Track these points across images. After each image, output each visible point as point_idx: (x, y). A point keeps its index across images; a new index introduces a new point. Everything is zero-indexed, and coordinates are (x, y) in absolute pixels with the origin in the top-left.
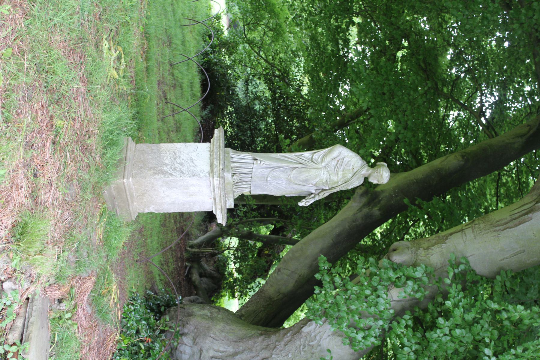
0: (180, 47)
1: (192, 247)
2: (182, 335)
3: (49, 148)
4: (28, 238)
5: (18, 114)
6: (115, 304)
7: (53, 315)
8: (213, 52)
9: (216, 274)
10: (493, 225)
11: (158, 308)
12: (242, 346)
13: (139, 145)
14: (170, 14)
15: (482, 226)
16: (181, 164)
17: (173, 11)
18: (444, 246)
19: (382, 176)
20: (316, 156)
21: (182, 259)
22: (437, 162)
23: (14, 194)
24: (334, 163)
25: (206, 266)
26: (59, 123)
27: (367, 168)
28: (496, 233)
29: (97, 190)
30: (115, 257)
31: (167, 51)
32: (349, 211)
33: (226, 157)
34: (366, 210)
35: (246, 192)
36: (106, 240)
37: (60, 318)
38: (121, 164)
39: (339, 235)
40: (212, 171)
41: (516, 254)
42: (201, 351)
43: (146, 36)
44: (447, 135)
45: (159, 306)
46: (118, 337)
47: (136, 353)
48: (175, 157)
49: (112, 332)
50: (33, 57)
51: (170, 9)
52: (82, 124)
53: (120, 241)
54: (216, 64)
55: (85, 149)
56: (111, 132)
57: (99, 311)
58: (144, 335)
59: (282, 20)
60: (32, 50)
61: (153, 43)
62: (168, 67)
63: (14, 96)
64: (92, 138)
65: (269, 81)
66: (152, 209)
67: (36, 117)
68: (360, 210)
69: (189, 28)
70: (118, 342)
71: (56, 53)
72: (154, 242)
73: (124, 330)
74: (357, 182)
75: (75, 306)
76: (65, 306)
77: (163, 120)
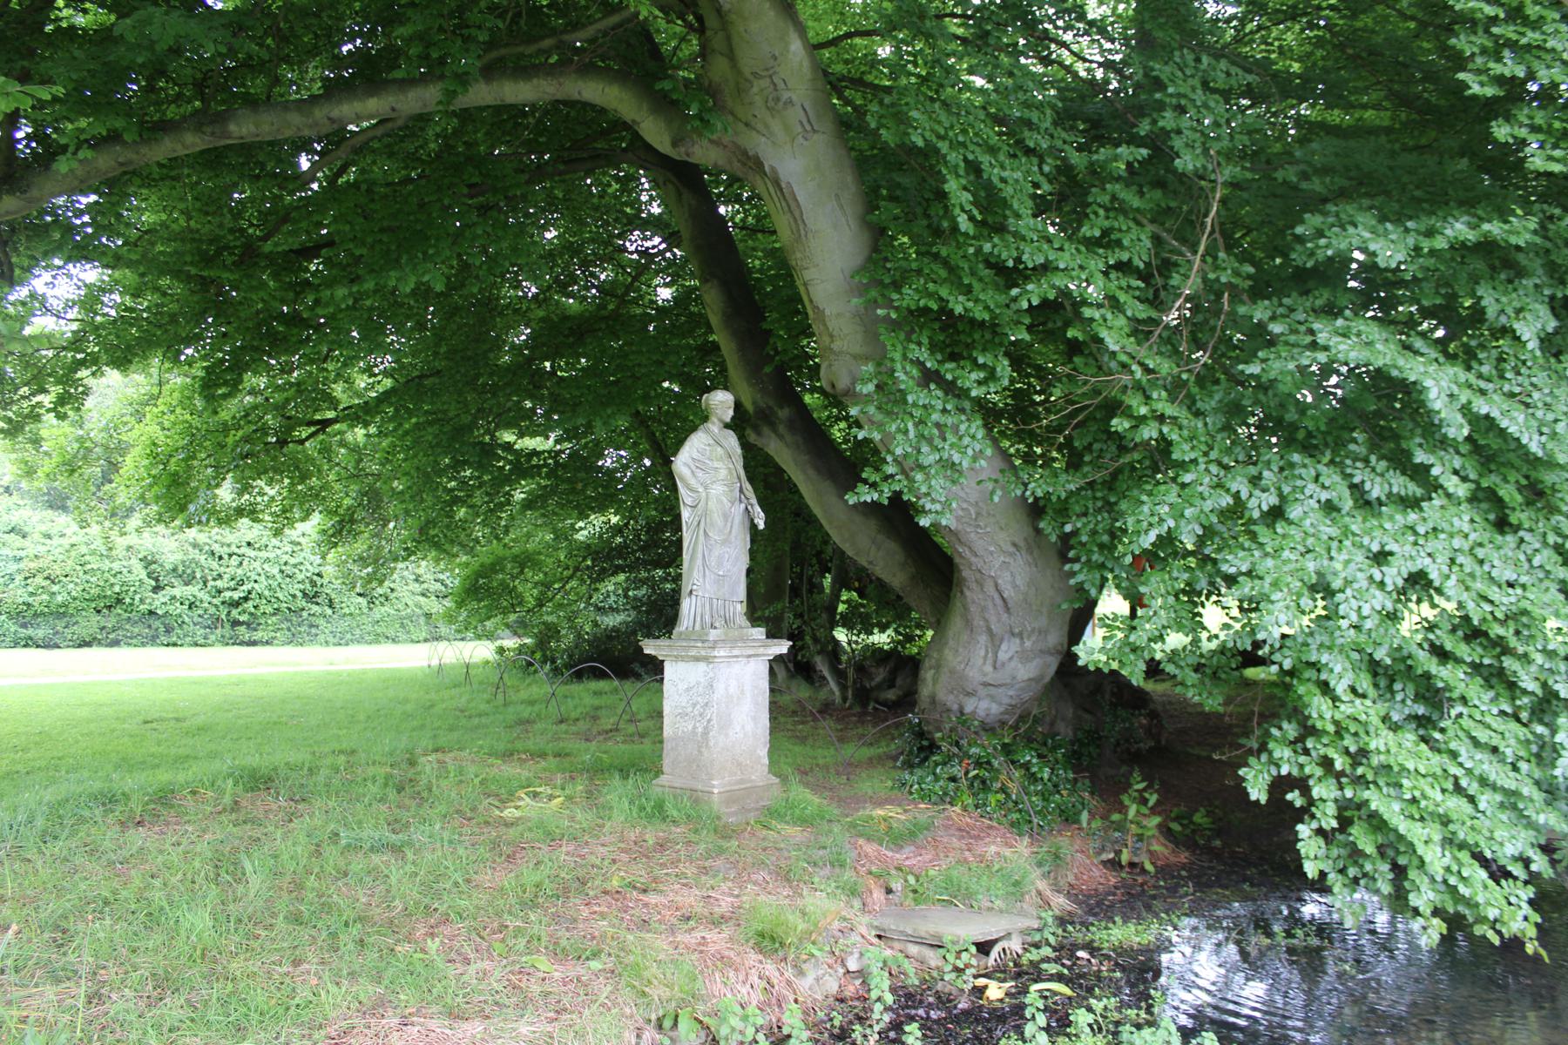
0: (536, 708)
1: (845, 699)
2: (962, 714)
3: (652, 898)
4: (780, 931)
5: (594, 938)
6: (906, 811)
7: (909, 901)
8: (553, 661)
9: (891, 664)
10: (798, 239)
11: (923, 749)
12: (978, 622)
13: (665, 769)
14: (483, 720)
15: (799, 255)
16: (694, 705)
17: (480, 715)
18: (827, 312)
19: (721, 402)
20: (688, 501)
21: (864, 713)
22: (715, 320)
23: (712, 949)
24: (700, 474)
25: (878, 679)
26: (615, 883)
27: (709, 425)
28: (810, 235)
29: (725, 832)
30: (836, 811)
31: (539, 726)
32: (783, 452)
33: (687, 637)
34: (782, 429)
35: (741, 608)
36: (804, 821)
37: (915, 891)
38: (697, 798)
39: (818, 471)
40: (706, 659)
41: (842, 207)
42: (986, 685)
43: (507, 755)
44: (681, 301)
45: (921, 749)
46: (957, 809)
47: (984, 782)
48: (683, 715)
49: (949, 818)
50: (510, 913)
51: (476, 721)
52: (623, 851)
53: (807, 798)
54: (570, 656)
55: (661, 846)
56: (642, 808)
57: (912, 834)
58: (957, 770)
59: (508, 553)
60: (499, 915)
61: (519, 745)
62: (563, 727)
63: (564, 942)
64: (647, 837)
65: (602, 575)
66: (763, 752)
67: (601, 914)
68: (781, 437)
69: (511, 692)
70: (965, 809)
71: (507, 880)
72: (825, 755)
73: (946, 798)
74: (732, 440)
75: (899, 869)
76: (897, 885)
77: (642, 736)
